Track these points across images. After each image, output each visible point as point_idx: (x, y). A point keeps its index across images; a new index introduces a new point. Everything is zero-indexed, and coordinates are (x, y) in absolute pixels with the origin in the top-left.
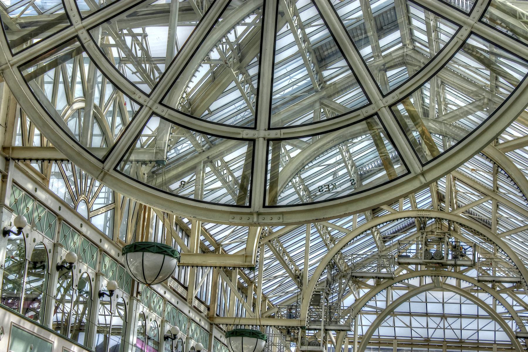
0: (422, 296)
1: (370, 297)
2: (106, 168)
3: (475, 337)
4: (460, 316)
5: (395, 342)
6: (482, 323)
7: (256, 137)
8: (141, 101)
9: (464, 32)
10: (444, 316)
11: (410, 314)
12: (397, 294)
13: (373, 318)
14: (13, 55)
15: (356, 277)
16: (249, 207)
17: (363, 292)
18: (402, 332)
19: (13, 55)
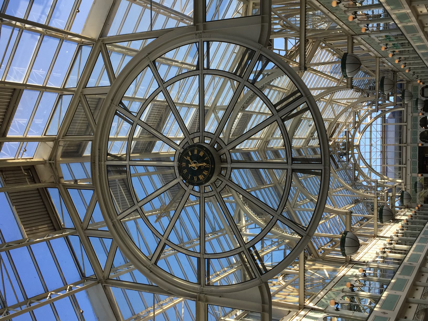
0: (363, 154)
1: (364, 175)
2: (305, 235)
3: (380, 132)
4: (371, 138)
5: (383, 165)
6: (373, 129)
7: (291, 169)
8: (276, 220)
9: (247, 83)
10: (371, 145)
11: (370, 159)
12: (362, 165)
13: (373, 174)
14: (256, 277)
15: (355, 179)
16: (322, 170)
17: (361, 178)
18: (379, 162)
19: (256, 277)
